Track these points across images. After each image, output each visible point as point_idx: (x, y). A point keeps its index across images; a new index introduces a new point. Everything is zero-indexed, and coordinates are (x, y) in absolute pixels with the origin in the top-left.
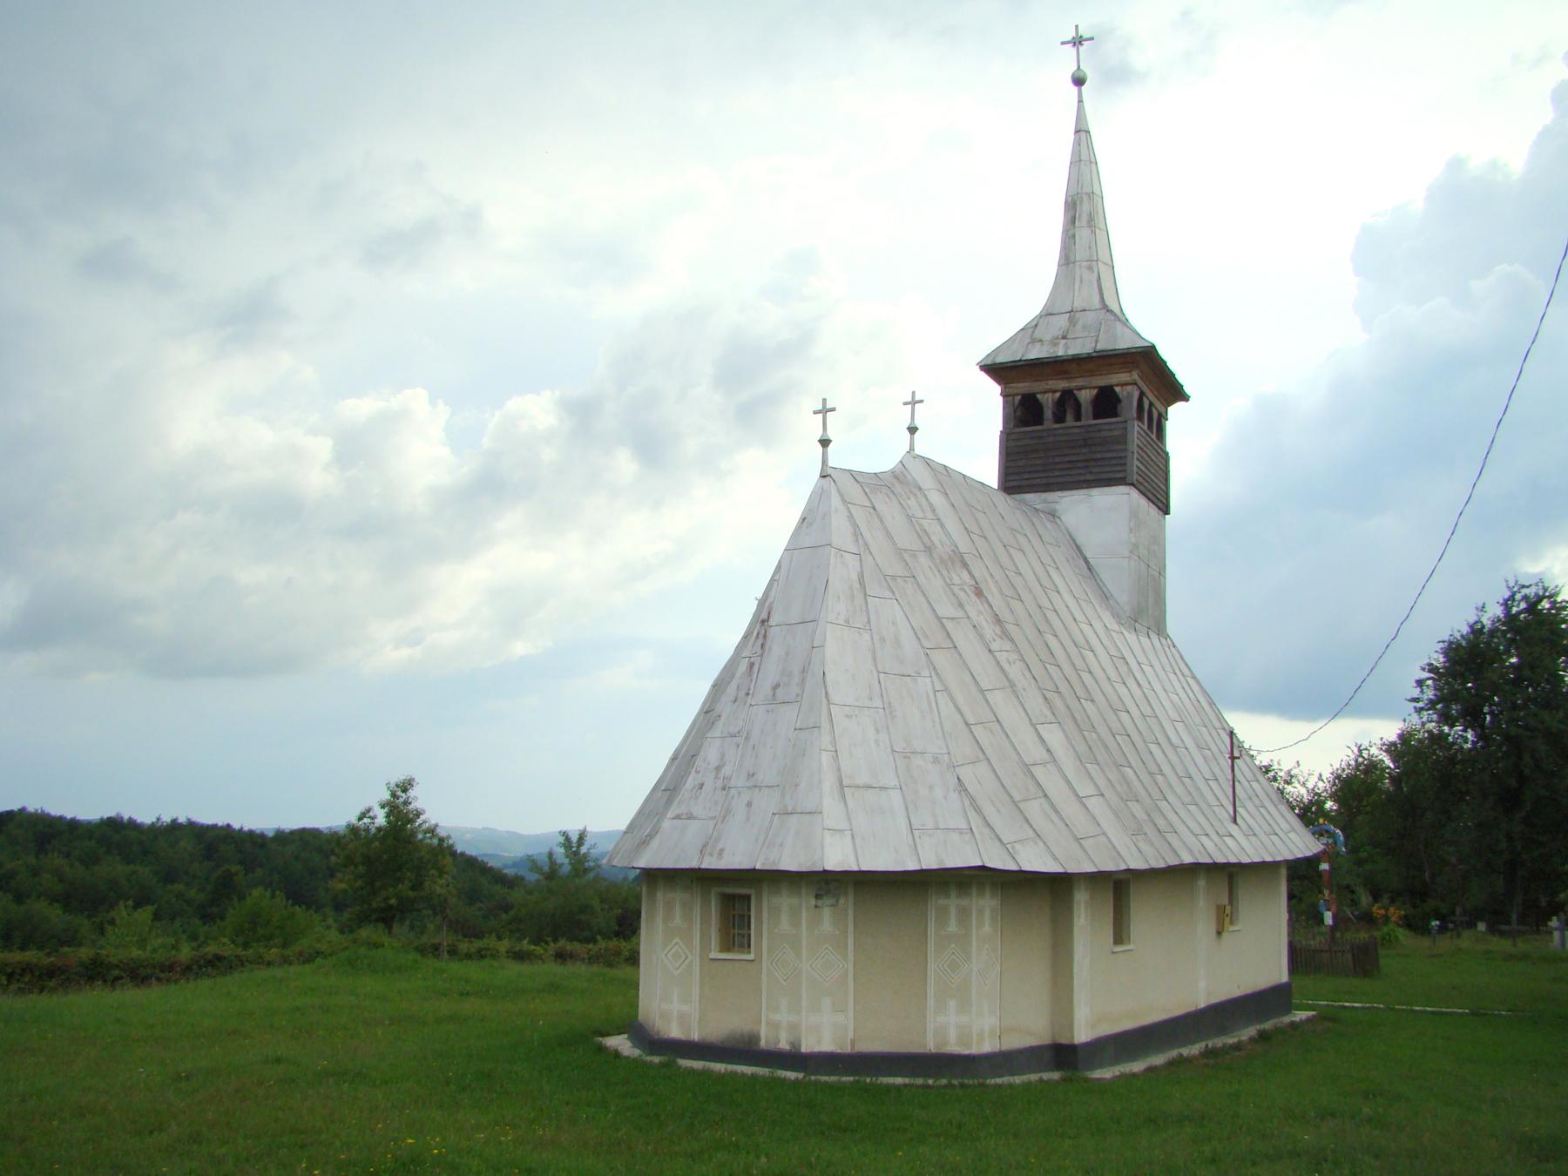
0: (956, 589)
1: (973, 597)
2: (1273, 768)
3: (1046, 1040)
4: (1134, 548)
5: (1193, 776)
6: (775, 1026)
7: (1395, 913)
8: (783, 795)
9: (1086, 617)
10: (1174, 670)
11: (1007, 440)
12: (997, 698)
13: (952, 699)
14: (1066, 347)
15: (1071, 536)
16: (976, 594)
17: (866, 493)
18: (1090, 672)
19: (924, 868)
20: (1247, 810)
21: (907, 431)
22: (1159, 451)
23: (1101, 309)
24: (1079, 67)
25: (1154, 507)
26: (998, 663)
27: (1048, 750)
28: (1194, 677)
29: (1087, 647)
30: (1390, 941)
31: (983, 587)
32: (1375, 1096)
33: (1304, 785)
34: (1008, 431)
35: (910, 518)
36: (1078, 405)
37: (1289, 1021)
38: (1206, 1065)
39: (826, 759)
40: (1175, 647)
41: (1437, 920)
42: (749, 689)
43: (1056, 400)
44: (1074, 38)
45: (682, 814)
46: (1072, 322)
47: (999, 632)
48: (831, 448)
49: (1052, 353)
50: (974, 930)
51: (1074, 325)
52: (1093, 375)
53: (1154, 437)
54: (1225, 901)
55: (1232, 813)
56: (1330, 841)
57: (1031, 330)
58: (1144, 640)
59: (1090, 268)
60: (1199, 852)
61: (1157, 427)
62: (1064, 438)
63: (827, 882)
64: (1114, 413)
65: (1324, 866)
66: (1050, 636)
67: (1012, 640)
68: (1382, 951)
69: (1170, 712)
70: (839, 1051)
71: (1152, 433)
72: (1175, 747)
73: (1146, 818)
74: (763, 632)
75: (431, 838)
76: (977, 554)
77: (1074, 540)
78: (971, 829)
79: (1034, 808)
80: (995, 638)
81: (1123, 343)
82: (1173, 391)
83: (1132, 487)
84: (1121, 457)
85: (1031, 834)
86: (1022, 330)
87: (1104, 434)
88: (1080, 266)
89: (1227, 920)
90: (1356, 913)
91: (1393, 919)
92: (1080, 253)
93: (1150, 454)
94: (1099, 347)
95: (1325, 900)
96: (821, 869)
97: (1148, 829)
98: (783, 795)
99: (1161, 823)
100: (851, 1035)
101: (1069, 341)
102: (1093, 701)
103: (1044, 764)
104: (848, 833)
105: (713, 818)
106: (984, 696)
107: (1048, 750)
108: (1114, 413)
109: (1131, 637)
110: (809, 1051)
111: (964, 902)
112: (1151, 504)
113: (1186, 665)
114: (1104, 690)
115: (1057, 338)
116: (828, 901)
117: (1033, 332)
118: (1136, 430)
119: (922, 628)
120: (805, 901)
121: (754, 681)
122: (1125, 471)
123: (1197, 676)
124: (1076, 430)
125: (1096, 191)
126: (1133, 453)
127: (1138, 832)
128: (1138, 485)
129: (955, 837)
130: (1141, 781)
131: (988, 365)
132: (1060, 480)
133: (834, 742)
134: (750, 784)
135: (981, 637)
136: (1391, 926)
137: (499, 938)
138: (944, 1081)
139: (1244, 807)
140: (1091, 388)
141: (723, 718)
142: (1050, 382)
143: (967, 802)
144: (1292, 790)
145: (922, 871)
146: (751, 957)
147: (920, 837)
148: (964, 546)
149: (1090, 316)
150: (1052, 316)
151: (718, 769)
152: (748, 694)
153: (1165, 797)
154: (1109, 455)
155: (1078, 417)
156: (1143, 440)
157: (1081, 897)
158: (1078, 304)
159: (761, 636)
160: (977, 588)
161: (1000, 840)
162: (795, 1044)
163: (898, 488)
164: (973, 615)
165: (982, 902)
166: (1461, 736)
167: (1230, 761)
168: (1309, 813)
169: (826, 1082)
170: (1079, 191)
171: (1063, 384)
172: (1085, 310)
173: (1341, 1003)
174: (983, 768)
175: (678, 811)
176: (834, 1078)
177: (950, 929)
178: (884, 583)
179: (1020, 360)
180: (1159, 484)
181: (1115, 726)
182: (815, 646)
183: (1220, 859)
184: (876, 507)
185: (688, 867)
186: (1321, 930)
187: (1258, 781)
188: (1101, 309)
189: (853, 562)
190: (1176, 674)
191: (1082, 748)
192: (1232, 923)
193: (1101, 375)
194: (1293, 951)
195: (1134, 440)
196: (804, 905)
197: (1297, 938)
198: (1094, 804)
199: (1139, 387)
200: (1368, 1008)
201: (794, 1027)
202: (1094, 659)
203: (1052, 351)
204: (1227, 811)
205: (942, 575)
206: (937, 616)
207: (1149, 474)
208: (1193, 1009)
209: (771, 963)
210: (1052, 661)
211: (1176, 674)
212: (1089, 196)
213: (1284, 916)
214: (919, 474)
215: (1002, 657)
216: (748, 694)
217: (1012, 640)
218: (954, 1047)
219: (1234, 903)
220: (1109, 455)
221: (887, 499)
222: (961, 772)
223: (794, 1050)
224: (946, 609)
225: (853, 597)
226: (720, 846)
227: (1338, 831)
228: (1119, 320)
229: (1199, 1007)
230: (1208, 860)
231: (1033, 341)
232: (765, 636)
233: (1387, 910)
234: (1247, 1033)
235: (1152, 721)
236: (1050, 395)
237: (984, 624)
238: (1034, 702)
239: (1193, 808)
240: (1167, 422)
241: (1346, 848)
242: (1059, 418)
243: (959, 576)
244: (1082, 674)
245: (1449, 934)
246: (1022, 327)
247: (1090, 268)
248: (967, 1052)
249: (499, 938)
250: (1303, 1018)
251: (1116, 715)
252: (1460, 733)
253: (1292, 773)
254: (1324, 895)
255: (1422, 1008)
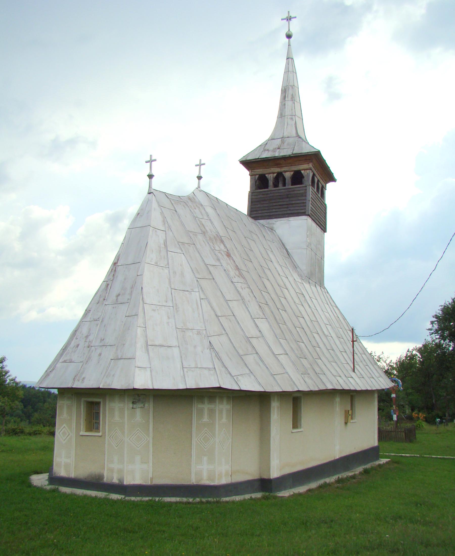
0: (217, 252)
1: (225, 257)
2: (372, 354)
3: (256, 477)
4: (309, 245)
5: (334, 349)
6: (112, 470)
7: (422, 415)
8: (117, 350)
9: (285, 274)
10: (327, 303)
11: (252, 196)
12: (233, 305)
13: (209, 303)
14: (280, 153)
15: (280, 240)
16: (227, 256)
17: (172, 204)
18: (285, 298)
19: (188, 388)
20: (360, 367)
21: (197, 178)
22: (322, 202)
23: (296, 137)
24: (289, 30)
25: (319, 228)
26: (236, 288)
27: (260, 331)
28: (337, 307)
29: (284, 287)
30: (420, 427)
31: (231, 252)
32: (421, 505)
33: (385, 362)
34: (253, 191)
35: (195, 218)
36: (284, 179)
37: (378, 464)
38: (337, 488)
39: (139, 331)
40: (328, 293)
41: (439, 418)
42: (105, 297)
43: (274, 177)
44: (287, 17)
45: (67, 360)
46: (283, 142)
47: (237, 273)
48: (154, 179)
49: (273, 155)
50: (217, 421)
51: (284, 143)
52: (291, 166)
53: (320, 196)
54: (349, 408)
55: (352, 367)
56: (396, 385)
57: (264, 146)
58: (313, 288)
59: (292, 119)
60: (336, 384)
61: (322, 192)
62: (277, 194)
63: (139, 395)
64: (301, 183)
65: (393, 395)
66: (266, 280)
67: (244, 278)
68: (417, 432)
69: (324, 320)
70: (144, 484)
71: (319, 194)
72: (326, 336)
73: (309, 366)
74: (114, 269)
75: (13, 383)
76: (230, 238)
77: (281, 241)
78: (215, 368)
79: (250, 359)
80: (235, 276)
81: (305, 150)
82: (330, 178)
83: (308, 216)
84: (304, 203)
85: (248, 371)
86: (260, 146)
87: (295, 192)
88: (287, 118)
89: (350, 417)
90: (406, 416)
91: (421, 418)
92: (288, 111)
93: (318, 204)
94: (294, 152)
95: (394, 410)
96: (133, 388)
97: (310, 371)
98: (117, 350)
99: (318, 370)
100: (150, 475)
101: (281, 150)
102: (285, 311)
103: (257, 338)
104: (149, 370)
105: (81, 362)
106: (227, 303)
107: (260, 331)
108: (301, 183)
109: (307, 286)
110: (128, 484)
111: (212, 406)
112: (318, 226)
113: (333, 301)
114: (292, 307)
115: (276, 149)
116: (140, 405)
117: (265, 147)
118: (311, 191)
119: (196, 268)
120: (127, 405)
121: (108, 293)
122: (305, 209)
123: (338, 306)
124: (283, 191)
125: (296, 85)
126: (309, 201)
127: (305, 373)
128: (311, 216)
129: (206, 372)
130: (308, 350)
131: (243, 161)
132: (276, 213)
133: (145, 323)
134: (101, 344)
135: (228, 275)
136: (420, 421)
137: (44, 426)
138: (198, 500)
139: (358, 365)
140: (290, 171)
141: (91, 312)
142: (272, 169)
143: (214, 355)
144: (381, 364)
145: (187, 389)
146: (100, 434)
147: (187, 372)
148: (222, 233)
149: (291, 140)
150: (274, 140)
151: (87, 337)
152: (104, 299)
153: (320, 358)
154: (298, 202)
155: (284, 185)
156: (314, 196)
157: (275, 404)
158: (286, 134)
159: (113, 271)
160: (228, 253)
161: (230, 374)
162: (121, 480)
163: (190, 203)
164: (224, 264)
165: (221, 406)
166: (448, 344)
167: (352, 343)
168: (388, 373)
169: (134, 501)
170: (288, 85)
171: (278, 170)
172: (288, 137)
173: (401, 454)
174: (224, 338)
175: (65, 359)
176: (139, 499)
177: (204, 420)
178: (178, 246)
179: (258, 158)
180: (322, 217)
181: (297, 324)
182: (139, 275)
183: (346, 388)
184: (177, 210)
185: (66, 387)
186: (391, 423)
187: (365, 354)
188: (296, 137)
189: (161, 235)
190: (328, 304)
191: (278, 332)
192: (352, 419)
193: (295, 165)
194: (380, 432)
195: (310, 195)
196: (126, 407)
197: (381, 426)
198: (282, 358)
199: (312, 171)
200: (412, 457)
201: (120, 471)
202: (287, 292)
203: (273, 154)
204: (350, 367)
205: (209, 245)
206: (205, 264)
207: (317, 212)
208: (332, 459)
209: (110, 437)
210: (265, 290)
211: (328, 304)
212: (292, 87)
213: (377, 417)
214: (200, 198)
215: (238, 286)
216: (104, 299)
217: (244, 278)
218: (206, 481)
219: (353, 409)
220: (298, 202)
221: (183, 208)
222: (212, 339)
223: (120, 484)
224: (211, 261)
225: (160, 251)
226: (83, 376)
227: (399, 380)
228: (304, 141)
229: (336, 458)
230: (340, 388)
231: (265, 150)
232: (115, 271)
233: (418, 414)
234: (359, 469)
235: (315, 324)
236: (272, 175)
237: (230, 270)
238: (254, 308)
239: (334, 364)
240: (326, 191)
241: (402, 388)
242: (276, 185)
243: (219, 247)
244: (281, 298)
245: (443, 424)
246: (260, 145)
247: (292, 119)
248: (212, 484)
249: (44, 426)
250: (384, 462)
251: (297, 319)
252: (448, 343)
253: (380, 357)
254: (393, 408)
255: (436, 456)
